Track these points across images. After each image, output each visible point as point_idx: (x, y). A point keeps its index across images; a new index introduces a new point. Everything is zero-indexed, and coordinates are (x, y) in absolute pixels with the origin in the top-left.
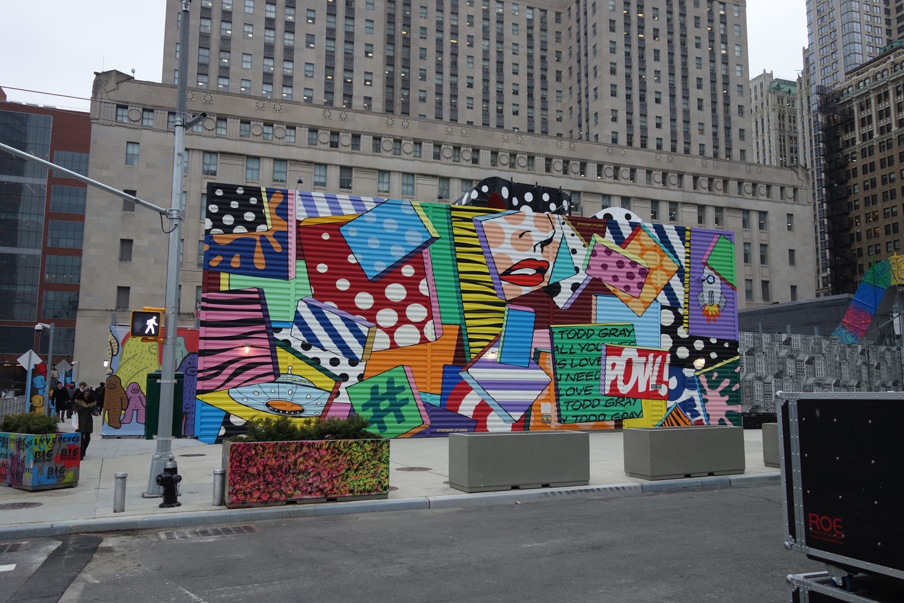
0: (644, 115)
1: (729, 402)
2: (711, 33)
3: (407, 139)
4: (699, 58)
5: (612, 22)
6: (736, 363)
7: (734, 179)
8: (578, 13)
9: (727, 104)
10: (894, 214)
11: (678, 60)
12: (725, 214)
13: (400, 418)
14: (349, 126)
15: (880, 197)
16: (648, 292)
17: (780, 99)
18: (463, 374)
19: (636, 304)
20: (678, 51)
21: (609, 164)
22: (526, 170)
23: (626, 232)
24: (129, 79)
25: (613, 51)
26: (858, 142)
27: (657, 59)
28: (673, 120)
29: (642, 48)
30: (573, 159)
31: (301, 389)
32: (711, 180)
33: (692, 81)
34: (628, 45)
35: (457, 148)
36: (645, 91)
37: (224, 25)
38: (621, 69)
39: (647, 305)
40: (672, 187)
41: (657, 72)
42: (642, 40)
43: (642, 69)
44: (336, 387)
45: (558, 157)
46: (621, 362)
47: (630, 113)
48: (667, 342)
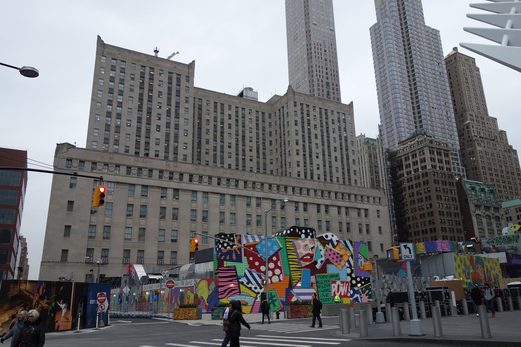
0: (311, 163)
1: (368, 298)
2: (340, 127)
3: (205, 176)
4: (334, 138)
5: (296, 121)
6: (370, 285)
7: (353, 194)
8: (280, 115)
9: (348, 159)
10: (423, 209)
11: (325, 139)
12: (350, 210)
13: (275, 306)
14: (178, 169)
15: (422, 184)
16: (343, 263)
17: (369, 148)
18: (291, 291)
19: (339, 266)
20: (325, 135)
21: (297, 187)
22: (260, 190)
23: (335, 243)
24: (74, 147)
25: (297, 134)
26: (405, 175)
27: (316, 138)
28: (324, 166)
29: (309, 133)
30: (281, 185)
31: (247, 297)
32: (343, 194)
33: (332, 148)
34: (303, 132)
35: (228, 180)
36: (311, 152)
37: (117, 120)
38: (301, 143)
39: (343, 267)
40: (326, 198)
41: (317, 144)
42: (309, 129)
43: (310, 143)
44: (256, 296)
45: (274, 184)
46: (336, 286)
47: (305, 163)
48: (349, 279)
